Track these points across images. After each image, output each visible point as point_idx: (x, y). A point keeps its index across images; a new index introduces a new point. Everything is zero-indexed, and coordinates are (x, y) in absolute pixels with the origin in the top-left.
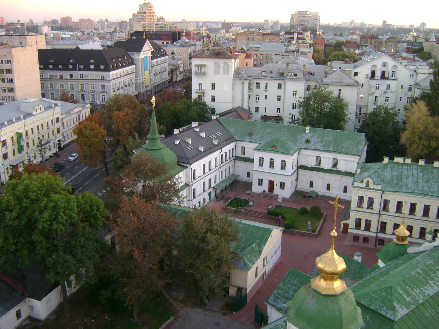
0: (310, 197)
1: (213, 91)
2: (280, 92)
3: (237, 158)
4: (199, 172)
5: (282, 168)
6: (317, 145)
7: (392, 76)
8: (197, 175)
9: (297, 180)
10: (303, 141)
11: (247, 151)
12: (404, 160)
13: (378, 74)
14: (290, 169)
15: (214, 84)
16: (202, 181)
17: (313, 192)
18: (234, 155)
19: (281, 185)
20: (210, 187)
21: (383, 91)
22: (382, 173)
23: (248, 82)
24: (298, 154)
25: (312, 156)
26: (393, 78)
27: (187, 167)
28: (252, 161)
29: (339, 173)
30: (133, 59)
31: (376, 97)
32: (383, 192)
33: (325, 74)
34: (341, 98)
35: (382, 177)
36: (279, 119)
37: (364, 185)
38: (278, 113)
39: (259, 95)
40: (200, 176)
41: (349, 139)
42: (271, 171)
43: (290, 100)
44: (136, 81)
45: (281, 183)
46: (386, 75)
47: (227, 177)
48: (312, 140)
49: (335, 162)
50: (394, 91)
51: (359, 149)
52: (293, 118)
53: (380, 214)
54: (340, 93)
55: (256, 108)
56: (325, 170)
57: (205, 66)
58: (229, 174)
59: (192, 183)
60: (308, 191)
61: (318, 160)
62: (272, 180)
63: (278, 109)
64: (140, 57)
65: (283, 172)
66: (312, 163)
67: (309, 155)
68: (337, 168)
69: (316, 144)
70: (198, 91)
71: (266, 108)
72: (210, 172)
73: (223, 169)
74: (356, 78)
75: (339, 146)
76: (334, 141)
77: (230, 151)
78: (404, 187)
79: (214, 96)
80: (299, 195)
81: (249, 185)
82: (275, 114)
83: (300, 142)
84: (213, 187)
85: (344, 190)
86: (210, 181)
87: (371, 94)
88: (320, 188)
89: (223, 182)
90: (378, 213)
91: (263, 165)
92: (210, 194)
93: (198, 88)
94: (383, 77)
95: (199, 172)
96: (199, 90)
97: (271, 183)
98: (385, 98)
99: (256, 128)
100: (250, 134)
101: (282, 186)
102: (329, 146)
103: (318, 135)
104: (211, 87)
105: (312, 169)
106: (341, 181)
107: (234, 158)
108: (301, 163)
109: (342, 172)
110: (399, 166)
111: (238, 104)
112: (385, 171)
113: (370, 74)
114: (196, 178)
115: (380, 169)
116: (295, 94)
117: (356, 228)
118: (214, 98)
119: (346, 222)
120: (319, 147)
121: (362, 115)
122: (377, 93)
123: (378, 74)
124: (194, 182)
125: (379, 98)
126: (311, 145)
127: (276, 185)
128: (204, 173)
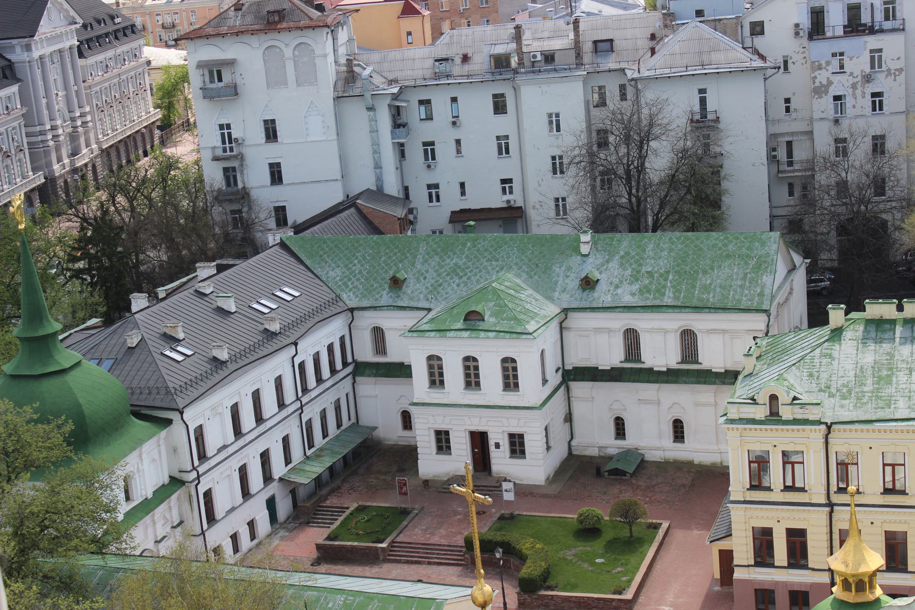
0: (617, 472)
1: (272, 146)
2: (504, 124)
3: (361, 369)
4: (218, 433)
5: (468, 384)
6: (619, 291)
7: (887, 18)
8: (212, 444)
9: (569, 418)
10: (573, 283)
11: (391, 340)
12: (900, 308)
13: (836, 19)
14: (531, 388)
15: (273, 121)
16: (235, 464)
17: (628, 454)
18: (350, 360)
19: (512, 444)
20: (268, 478)
21: (857, 72)
22: (824, 361)
23: (388, 100)
24: (561, 329)
25: (610, 331)
26: (888, 25)
27: (168, 422)
28: (402, 371)
29: (706, 377)
30: (10, 65)
31: (837, 98)
32: (829, 427)
33: (652, 44)
34: (710, 117)
35: (824, 376)
36: (511, 217)
37: (761, 412)
38: (508, 197)
39: (432, 143)
40: (225, 447)
41: (728, 256)
42: (472, 397)
43: (538, 147)
44: (34, 139)
45: (512, 436)
46: (865, 18)
47: (331, 436)
48: (603, 277)
49: (688, 339)
50: (900, 70)
51: (763, 287)
52: (560, 205)
53: (831, 505)
54: (703, 101)
55: (429, 187)
56: (659, 372)
57: (231, 63)
58: (339, 425)
59: (194, 475)
60: (612, 451)
61: (632, 340)
62: (481, 428)
63: (504, 181)
64: (36, 54)
65: (511, 399)
66: (611, 355)
67: (598, 330)
68: (697, 362)
69: (617, 287)
70: (219, 152)
71: (462, 185)
72: (262, 428)
73: (312, 413)
74: (759, 42)
75: (694, 287)
76: (678, 272)
77: (330, 348)
78: (901, 403)
79: (278, 165)
80: (579, 470)
81: (407, 456)
82: (496, 200)
83: (564, 291)
84: (281, 479)
85: (675, 432)
86: (265, 457)
87: (820, 91)
88: (650, 439)
89: (318, 455)
90: (823, 500)
91: (442, 383)
92: (271, 504)
93: (219, 143)
94: (855, 26)
95: (218, 433)
96: (225, 150)
97: (479, 440)
98: (868, 100)
99: (415, 257)
100: (396, 283)
101: (517, 445)
102: (660, 292)
103: (622, 257)
104: (263, 135)
105: (614, 375)
106: (716, 405)
107: (350, 369)
108: (575, 360)
109: (717, 375)
110: (884, 331)
111: (364, 181)
112: (835, 354)
113: (806, 22)
114: (209, 454)
115: (818, 351)
116: (555, 122)
117: (757, 564)
118: (280, 172)
119: (724, 545)
120: (628, 300)
121: (796, 167)
122: (840, 85)
123: (836, 19)
124: (201, 470)
125: (849, 101)
126: (602, 295)
127: (497, 446)
128: (238, 432)
